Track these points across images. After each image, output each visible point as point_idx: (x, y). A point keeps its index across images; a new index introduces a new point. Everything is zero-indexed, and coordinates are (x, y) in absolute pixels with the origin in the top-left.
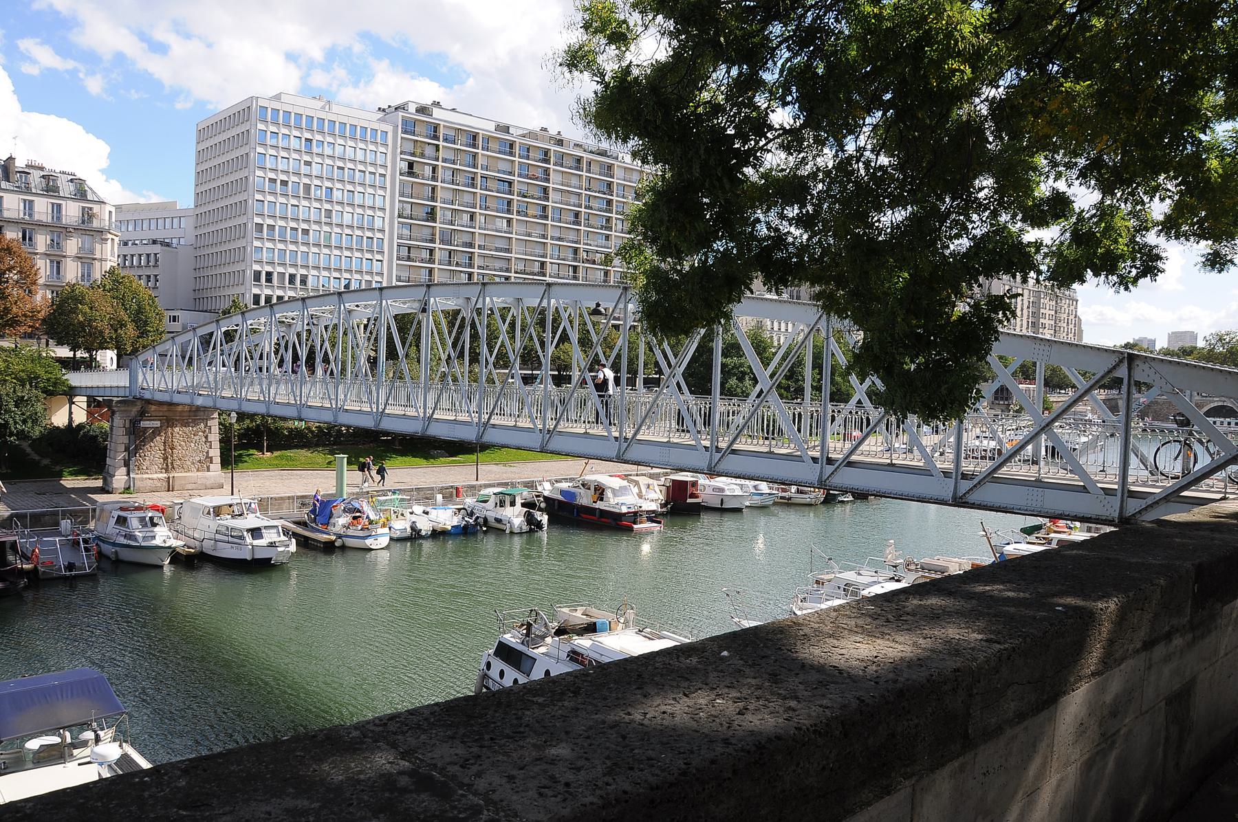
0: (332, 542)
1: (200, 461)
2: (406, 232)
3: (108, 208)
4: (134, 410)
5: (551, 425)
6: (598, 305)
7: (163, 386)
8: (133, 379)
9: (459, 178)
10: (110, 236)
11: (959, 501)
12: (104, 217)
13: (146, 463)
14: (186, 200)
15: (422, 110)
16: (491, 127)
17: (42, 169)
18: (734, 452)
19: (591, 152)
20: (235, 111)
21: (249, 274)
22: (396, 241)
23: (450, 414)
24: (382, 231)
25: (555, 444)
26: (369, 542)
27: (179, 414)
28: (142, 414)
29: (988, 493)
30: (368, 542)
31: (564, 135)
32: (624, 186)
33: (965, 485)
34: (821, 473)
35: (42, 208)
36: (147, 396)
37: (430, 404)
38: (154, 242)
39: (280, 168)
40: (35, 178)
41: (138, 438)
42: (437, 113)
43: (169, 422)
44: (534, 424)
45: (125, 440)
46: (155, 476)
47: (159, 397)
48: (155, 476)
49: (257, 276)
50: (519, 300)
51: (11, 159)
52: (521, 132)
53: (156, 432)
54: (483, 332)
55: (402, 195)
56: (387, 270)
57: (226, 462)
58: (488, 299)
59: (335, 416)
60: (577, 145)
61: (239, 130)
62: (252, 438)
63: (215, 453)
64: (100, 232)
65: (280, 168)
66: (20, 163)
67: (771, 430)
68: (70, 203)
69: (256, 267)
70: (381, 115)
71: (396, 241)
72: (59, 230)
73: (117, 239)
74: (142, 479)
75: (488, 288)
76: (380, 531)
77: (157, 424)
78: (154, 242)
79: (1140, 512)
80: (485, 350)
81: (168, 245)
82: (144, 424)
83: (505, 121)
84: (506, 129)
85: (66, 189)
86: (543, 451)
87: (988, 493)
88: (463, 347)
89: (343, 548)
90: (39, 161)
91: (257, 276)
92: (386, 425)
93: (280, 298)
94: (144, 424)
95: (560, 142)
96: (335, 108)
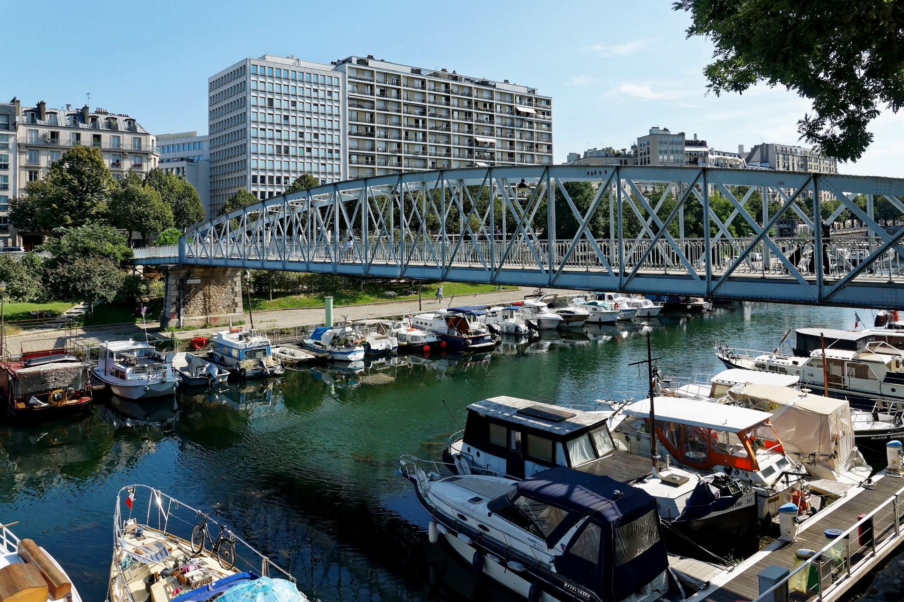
0: (325, 358)
1: (228, 306)
2: (355, 144)
3: (152, 137)
4: (183, 272)
5: (405, 262)
6: (523, 181)
7: (204, 255)
8: (181, 250)
9: (389, 107)
10: (153, 156)
11: (824, 301)
12: (149, 143)
13: (191, 309)
14: (203, 130)
15: (361, 62)
16: (409, 70)
17: (106, 113)
18: (638, 275)
19: (477, 83)
20: (226, 74)
21: (249, 178)
22: (348, 151)
23: (423, 260)
24: (338, 145)
25: (501, 277)
26: (350, 357)
27: (214, 273)
28: (188, 276)
29: (849, 294)
30: (350, 357)
31: (458, 73)
32: (358, 111)
33: (827, 290)
34: (708, 286)
35: (127, 142)
36: (191, 261)
37: (369, 256)
38: (182, 159)
39: (259, 105)
40: (102, 119)
41: (185, 294)
42: (371, 62)
43: (206, 281)
44: (485, 265)
45: (176, 293)
46: (197, 318)
47: (200, 262)
48: (197, 318)
49: (255, 179)
50: (461, 181)
51: (86, 108)
52: (429, 73)
53: (198, 288)
54: (401, 206)
55: (350, 120)
56: (340, 169)
57: (246, 307)
58: (445, 181)
59: (335, 268)
60: (466, 79)
61: (238, 81)
62: (265, 288)
63: (239, 300)
64: (147, 154)
65: (259, 105)
66: (92, 111)
67: (657, 260)
68: (125, 135)
69: (254, 173)
70: (333, 67)
71: (348, 151)
72: (119, 154)
73: (157, 159)
74: (188, 320)
75: (446, 174)
76: (358, 348)
77: (199, 281)
78: (182, 159)
79: (831, 294)
80: (404, 218)
81: (192, 161)
82: (190, 282)
83: (417, 66)
84: (418, 71)
85: (122, 125)
86: (493, 282)
87: (849, 294)
88: (333, 215)
89: (333, 361)
90: (104, 109)
91: (255, 179)
92: (374, 271)
93: (271, 193)
94: (190, 282)
95: (455, 78)
96: (302, 64)
